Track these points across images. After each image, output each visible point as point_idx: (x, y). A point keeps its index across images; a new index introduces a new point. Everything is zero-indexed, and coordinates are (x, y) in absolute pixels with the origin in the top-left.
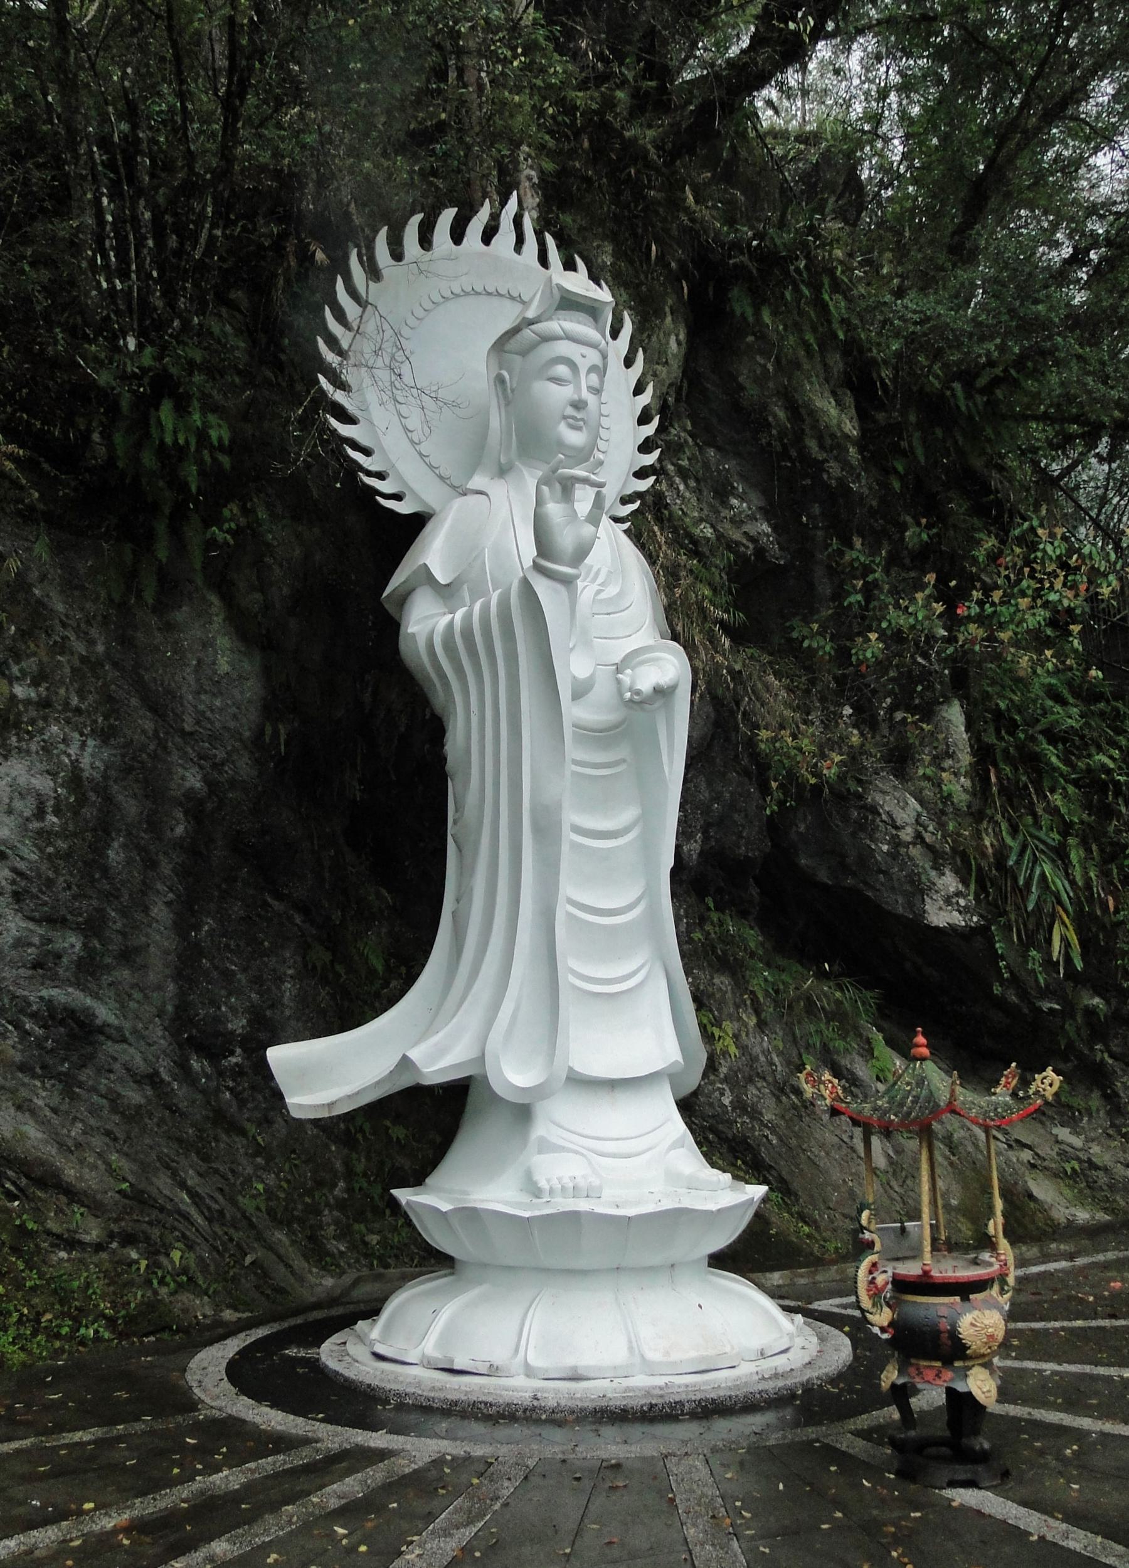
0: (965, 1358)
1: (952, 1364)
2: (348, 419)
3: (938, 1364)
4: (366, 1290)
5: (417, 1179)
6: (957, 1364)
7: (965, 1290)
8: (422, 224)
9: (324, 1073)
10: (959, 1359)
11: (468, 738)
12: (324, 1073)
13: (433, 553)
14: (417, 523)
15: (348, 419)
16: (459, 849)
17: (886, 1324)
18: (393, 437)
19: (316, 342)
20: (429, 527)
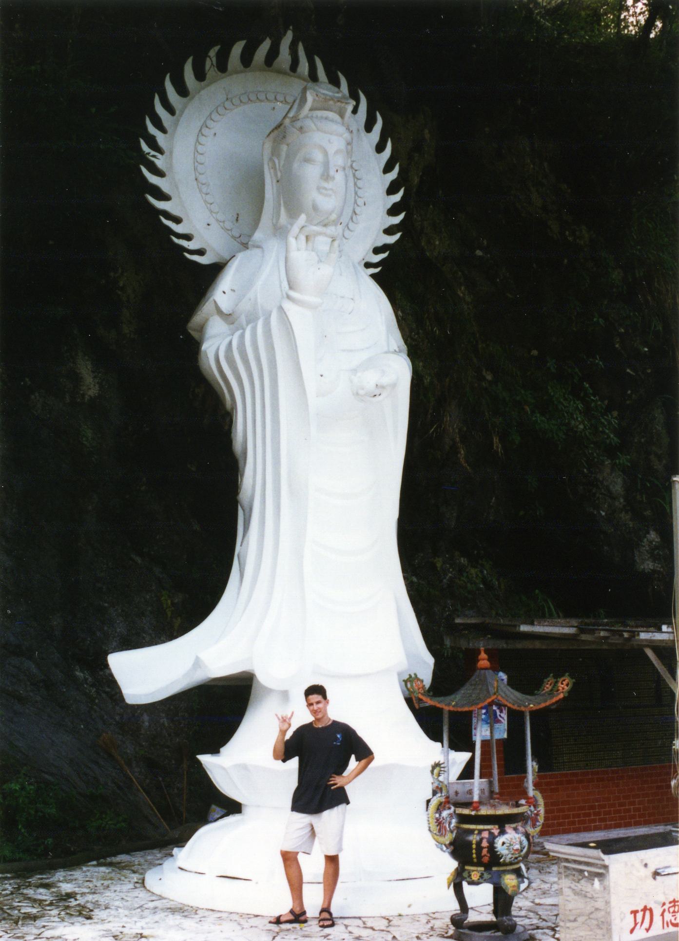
0: (499, 864)
1: (491, 869)
2: (165, 197)
3: (482, 869)
4: (176, 834)
5: (215, 750)
6: (494, 869)
7: (502, 821)
8: (218, 55)
9: (146, 674)
10: (495, 866)
11: (250, 431)
12: (146, 674)
13: (223, 293)
14: (216, 269)
15: (165, 197)
16: (244, 510)
17: (447, 842)
18: (195, 213)
19: (139, 142)
20: (227, 268)
